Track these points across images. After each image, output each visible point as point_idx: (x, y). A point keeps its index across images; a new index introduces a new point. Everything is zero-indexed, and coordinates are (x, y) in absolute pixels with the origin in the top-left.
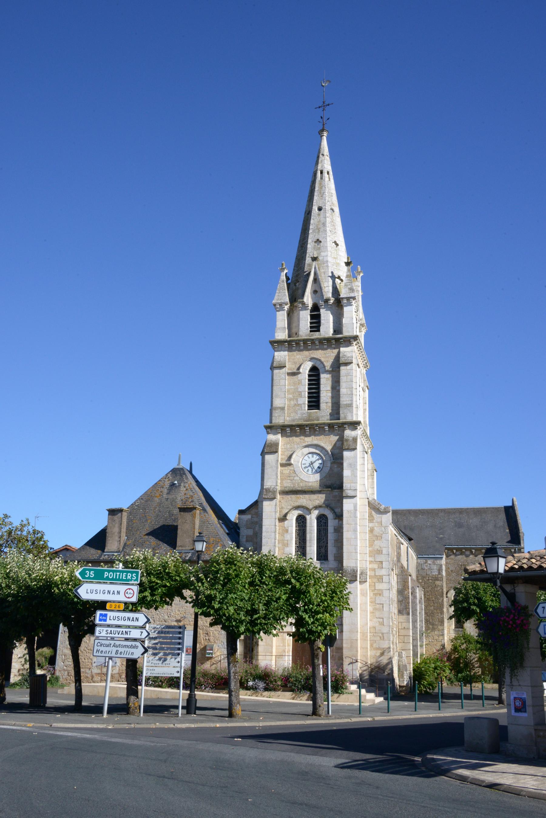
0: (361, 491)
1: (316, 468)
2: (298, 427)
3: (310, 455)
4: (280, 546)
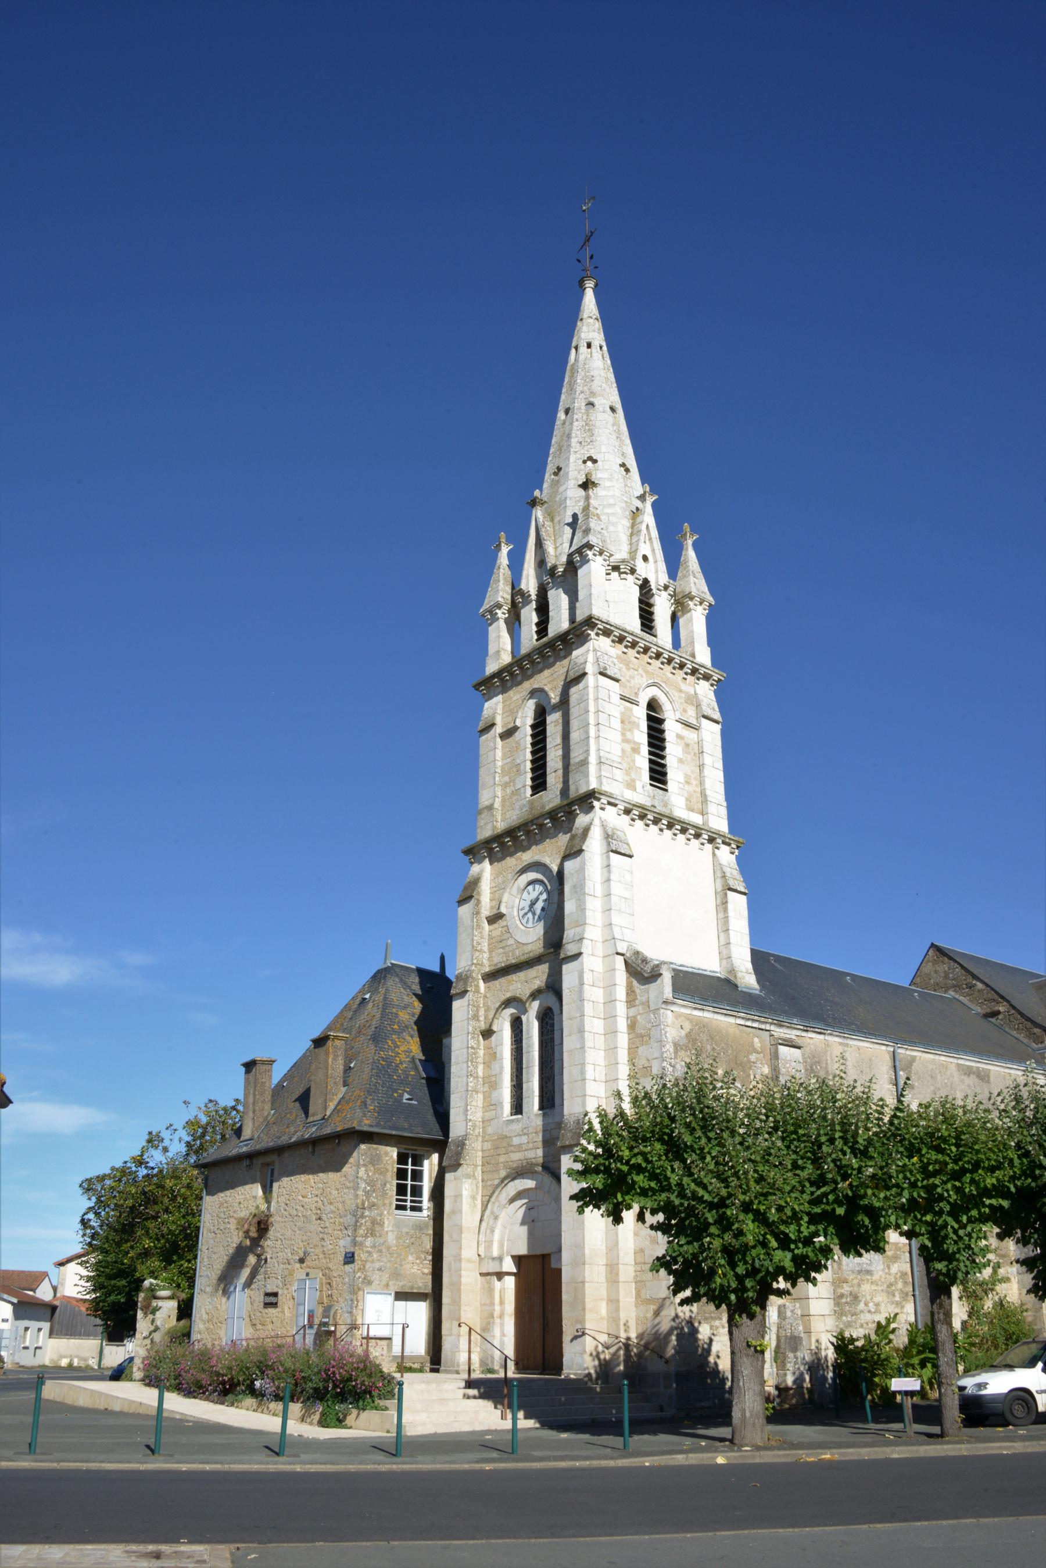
0: (607, 941)
1: (538, 912)
2: (507, 837)
3: (530, 888)
4: (485, 1090)
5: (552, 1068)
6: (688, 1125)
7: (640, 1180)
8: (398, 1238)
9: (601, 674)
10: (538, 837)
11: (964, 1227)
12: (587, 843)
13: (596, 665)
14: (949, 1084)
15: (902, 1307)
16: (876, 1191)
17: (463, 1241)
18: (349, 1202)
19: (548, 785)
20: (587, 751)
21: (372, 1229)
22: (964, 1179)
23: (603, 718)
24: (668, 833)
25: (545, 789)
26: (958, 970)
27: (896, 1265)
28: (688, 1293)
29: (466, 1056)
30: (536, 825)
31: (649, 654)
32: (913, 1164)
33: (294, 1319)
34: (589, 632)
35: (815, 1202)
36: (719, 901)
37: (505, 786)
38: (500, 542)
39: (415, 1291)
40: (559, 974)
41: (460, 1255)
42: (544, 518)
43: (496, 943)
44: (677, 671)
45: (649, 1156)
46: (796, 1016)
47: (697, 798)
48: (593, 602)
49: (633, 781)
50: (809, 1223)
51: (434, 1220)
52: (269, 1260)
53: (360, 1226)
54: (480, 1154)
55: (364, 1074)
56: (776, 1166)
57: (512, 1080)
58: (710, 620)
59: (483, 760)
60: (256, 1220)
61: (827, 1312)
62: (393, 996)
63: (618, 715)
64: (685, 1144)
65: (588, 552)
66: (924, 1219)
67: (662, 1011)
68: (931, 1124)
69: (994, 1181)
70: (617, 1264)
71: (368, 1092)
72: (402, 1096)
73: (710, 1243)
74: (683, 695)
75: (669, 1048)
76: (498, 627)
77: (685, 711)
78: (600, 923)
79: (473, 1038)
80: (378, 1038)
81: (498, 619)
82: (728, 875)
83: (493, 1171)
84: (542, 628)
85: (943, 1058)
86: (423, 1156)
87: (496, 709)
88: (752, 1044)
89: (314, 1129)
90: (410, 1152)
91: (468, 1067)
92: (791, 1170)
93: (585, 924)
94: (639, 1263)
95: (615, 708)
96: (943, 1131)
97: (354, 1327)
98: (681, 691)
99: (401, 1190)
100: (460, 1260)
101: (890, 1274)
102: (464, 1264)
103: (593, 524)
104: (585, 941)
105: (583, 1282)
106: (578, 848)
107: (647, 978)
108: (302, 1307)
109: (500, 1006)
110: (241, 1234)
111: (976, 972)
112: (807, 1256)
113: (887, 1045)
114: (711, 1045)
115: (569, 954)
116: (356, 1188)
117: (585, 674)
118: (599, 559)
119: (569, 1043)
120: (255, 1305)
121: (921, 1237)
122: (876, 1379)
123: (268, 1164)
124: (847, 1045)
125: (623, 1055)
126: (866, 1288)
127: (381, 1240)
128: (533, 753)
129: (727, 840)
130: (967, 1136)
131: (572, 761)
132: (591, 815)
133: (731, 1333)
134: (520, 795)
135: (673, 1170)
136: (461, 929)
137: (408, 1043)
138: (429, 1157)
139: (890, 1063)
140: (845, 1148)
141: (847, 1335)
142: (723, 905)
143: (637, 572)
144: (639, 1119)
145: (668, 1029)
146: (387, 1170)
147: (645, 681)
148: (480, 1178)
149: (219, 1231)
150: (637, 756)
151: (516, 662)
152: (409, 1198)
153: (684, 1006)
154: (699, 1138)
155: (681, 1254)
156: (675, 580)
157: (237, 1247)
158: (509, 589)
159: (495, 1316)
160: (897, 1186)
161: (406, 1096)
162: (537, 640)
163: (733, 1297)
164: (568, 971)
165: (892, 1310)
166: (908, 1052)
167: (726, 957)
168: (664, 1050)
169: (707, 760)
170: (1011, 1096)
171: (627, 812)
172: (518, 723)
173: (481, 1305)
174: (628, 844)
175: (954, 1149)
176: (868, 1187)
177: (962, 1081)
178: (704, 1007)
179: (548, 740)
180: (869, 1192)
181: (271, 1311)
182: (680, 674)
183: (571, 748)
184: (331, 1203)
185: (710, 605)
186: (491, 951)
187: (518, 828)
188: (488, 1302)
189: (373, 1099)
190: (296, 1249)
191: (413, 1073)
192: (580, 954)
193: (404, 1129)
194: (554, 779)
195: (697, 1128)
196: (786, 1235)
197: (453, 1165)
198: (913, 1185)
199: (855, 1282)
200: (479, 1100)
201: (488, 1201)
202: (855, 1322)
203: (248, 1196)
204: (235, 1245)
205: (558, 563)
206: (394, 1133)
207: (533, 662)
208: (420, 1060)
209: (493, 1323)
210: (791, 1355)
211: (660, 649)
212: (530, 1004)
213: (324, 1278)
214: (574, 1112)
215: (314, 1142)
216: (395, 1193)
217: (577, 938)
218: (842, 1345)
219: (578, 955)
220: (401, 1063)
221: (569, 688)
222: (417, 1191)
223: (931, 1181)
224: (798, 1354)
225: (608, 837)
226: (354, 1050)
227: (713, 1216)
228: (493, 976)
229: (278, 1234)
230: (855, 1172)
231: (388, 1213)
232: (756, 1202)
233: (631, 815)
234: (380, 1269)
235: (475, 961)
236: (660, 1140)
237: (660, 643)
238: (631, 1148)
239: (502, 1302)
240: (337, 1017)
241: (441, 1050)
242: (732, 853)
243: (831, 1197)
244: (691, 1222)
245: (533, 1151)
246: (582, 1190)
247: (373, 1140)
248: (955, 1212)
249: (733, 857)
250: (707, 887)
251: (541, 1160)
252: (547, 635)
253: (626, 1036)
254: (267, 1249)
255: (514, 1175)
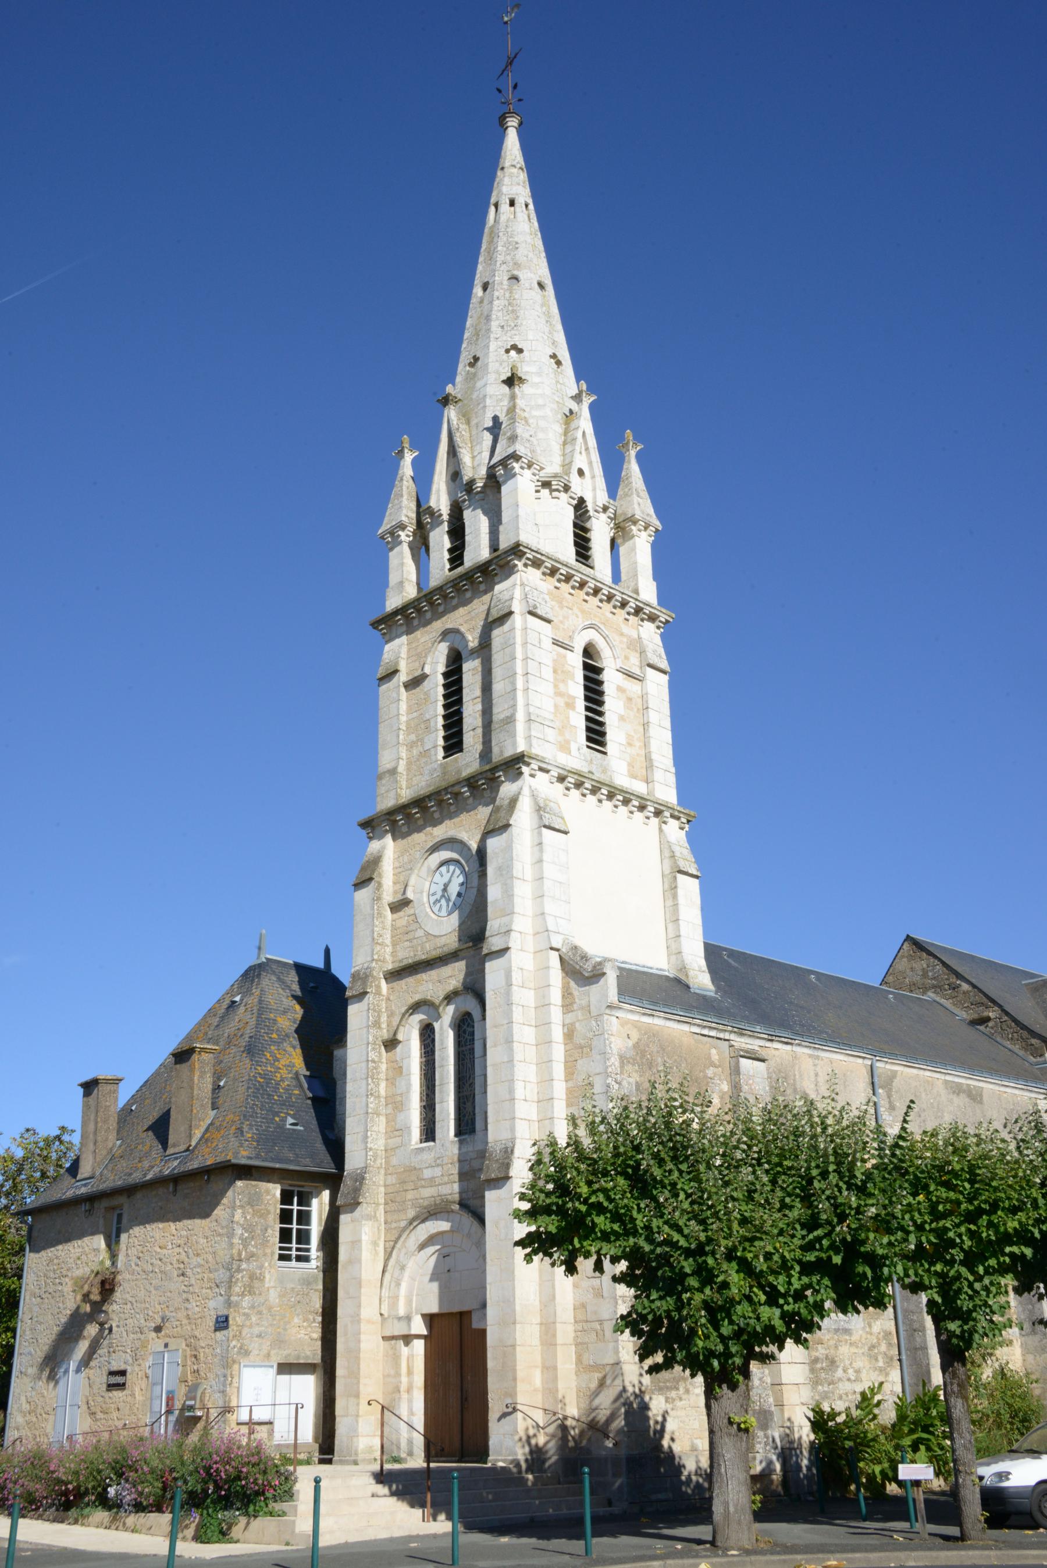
1: (453, 897)
2: (414, 807)
3: (444, 869)
5: (472, 1085)
6: (656, 1156)
7: (601, 1222)
8: (281, 1296)
9: (530, 613)
10: (453, 808)
11: (979, 1279)
12: (515, 816)
13: (524, 602)
14: (935, 1105)
15: (887, 1374)
16: (878, 1235)
17: (363, 1298)
18: (221, 1253)
19: (465, 746)
20: (514, 706)
21: (250, 1286)
22: (980, 1222)
23: (532, 666)
24: (608, 805)
25: (461, 750)
26: (939, 967)
27: (878, 1323)
28: (659, 1358)
29: (364, 1071)
30: (451, 793)
31: (586, 589)
32: (919, 1203)
33: (148, 1403)
34: (516, 562)
35: (808, 1247)
36: (667, 886)
37: (411, 746)
38: (403, 448)
39: (302, 1361)
40: (482, 972)
41: (358, 1315)
42: (459, 419)
43: (400, 935)
44: (618, 611)
45: (611, 1193)
46: (759, 1023)
47: (641, 762)
48: (520, 526)
49: (568, 742)
50: (801, 1273)
51: (325, 1271)
52: (114, 1329)
53: (236, 1283)
54: (382, 1189)
55: (238, 1094)
56: (761, 1205)
57: (421, 1100)
58: (654, 546)
59: (383, 714)
60: (99, 1278)
61: (801, 1380)
62: (270, 999)
63: (550, 663)
64: (654, 1179)
65: (515, 464)
66: (933, 1269)
67: (606, 1017)
68: (939, 1155)
69: (1016, 1224)
70: (554, 1323)
71: (245, 1116)
72: (284, 1120)
73: (690, 1299)
74: (625, 640)
75: (614, 1061)
76: (402, 553)
77: (627, 658)
78: (530, 913)
79: (374, 1049)
80: (252, 1050)
81: (401, 542)
82: (677, 854)
83: (399, 1211)
84: (456, 555)
85: (928, 1074)
86: (311, 1193)
87: (400, 653)
88: (709, 1057)
89: (176, 1163)
90: (296, 1189)
91: (368, 1084)
92: (779, 1210)
93: (513, 913)
94: (580, 1321)
95: (547, 654)
96: (955, 1164)
97: (227, 1410)
98: (622, 634)
99: (285, 1236)
100: (359, 1321)
101: (871, 1334)
102: (364, 1327)
103: (520, 430)
104: (513, 934)
105: (514, 1346)
106: (504, 822)
107: (588, 978)
108: (159, 1387)
109: (407, 1011)
110: (79, 1297)
111: (960, 970)
112: (798, 1314)
113: (864, 1058)
114: (663, 1057)
115: (495, 949)
116: (231, 1235)
117: (511, 613)
118: (527, 473)
119: (494, 1055)
120: (95, 1387)
121: (929, 1291)
122: (861, 1464)
123: (113, 1208)
124: (818, 1057)
125: (559, 1070)
126: (844, 1350)
127: (261, 1299)
128: (446, 707)
129: (676, 813)
130: (984, 1170)
131: (495, 718)
132: (519, 783)
133: (708, 1407)
134: (430, 757)
135: (639, 1210)
136: (358, 918)
137: (290, 1055)
138: (318, 1194)
139: (867, 1078)
140: (841, 1184)
141: (826, 1408)
142: (672, 889)
143: (572, 489)
144: (598, 1149)
145: (613, 1039)
146: (269, 1212)
147: (581, 623)
148: (383, 1220)
149: (47, 1295)
150: (571, 712)
151: (425, 596)
152: (294, 1245)
153: (631, 1011)
154: (670, 1171)
155: (652, 1310)
156: (614, 500)
157: (71, 1315)
158: (413, 506)
159: (402, 1389)
160: (902, 1228)
161: (290, 1120)
162: (450, 570)
163: (716, 1363)
164: (492, 969)
165: (875, 1378)
166: (888, 1067)
167: (675, 952)
168: (608, 1064)
169: (653, 717)
170: (1030, 1122)
171: (561, 779)
172: (427, 670)
173: (384, 1376)
174: (563, 818)
175: (967, 1185)
176: (868, 1230)
177: (951, 1101)
178: (654, 1013)
179: (465, 692)
180: (872, 1236)
181: (117, 1394)
182: (621, 613)
183: (494, 702)
184: (198, 1255)
185: (657, 530)
186: (394, 944)
187: (429, 797)
188: (392, 1372)
189: (250, 1125)
190: (151, 1313)
191: (297, 1092)
192: (507, 949)
193: (288, 1161)
194: (472, 738)
195: (667, 1159)
196: (774, 1288)
197: (350, 1204)
198: (920, 1228)
199: (832, 1343)
200: (380, 1125)
201: (393, 1248)
202: (833, 1393)
203: (86, 1249)
204: (69, 1312)
205: (476, 476)
206: (277, 1166)
207: (445, 597)
208: (305, 1076)
209: (400, 1398)
210: (760, 1434)
211: (598, 584)
212: (444, 1009)
213: (188, 1349)
214: (501, 1138)
215: (176, 1180)
216: (278, 1240)
217: (503, 930)
218: (820, 1422)
219: (505, 950)
220: (282, 1080)
221: (491, 630)
222: (304, 1237)
223: (941, 1223)
224: (769, 1432)
225: (540, 809)
226: (222, 1065)
227: (690, 1265)
228: (397, 974)
229: (128, 1296)
230: (853, 1213)
231: (270, 1265)
232: (741, 1249)
233: (566, 783)
234: (259, 1336)
235: (376, 957)
236: (624, 1174)
237: (599, 576)
238: (589, 1183)
239: (410, 1373)
240: (199, 1024)
241: (332, 1064)
242: (682, 829)
243: (825, 1242)
244: (665, 1272)
245: (449, 1186)
246: (529, 1234)
247: (251, 1175)
248: (970, 1260)
249: (683, 833)
250: (654, 869)
251: (457, 1197)
252: (462, 564)
253: (562, 1047)
254: (113, 1316)
255: (425, 1216)
